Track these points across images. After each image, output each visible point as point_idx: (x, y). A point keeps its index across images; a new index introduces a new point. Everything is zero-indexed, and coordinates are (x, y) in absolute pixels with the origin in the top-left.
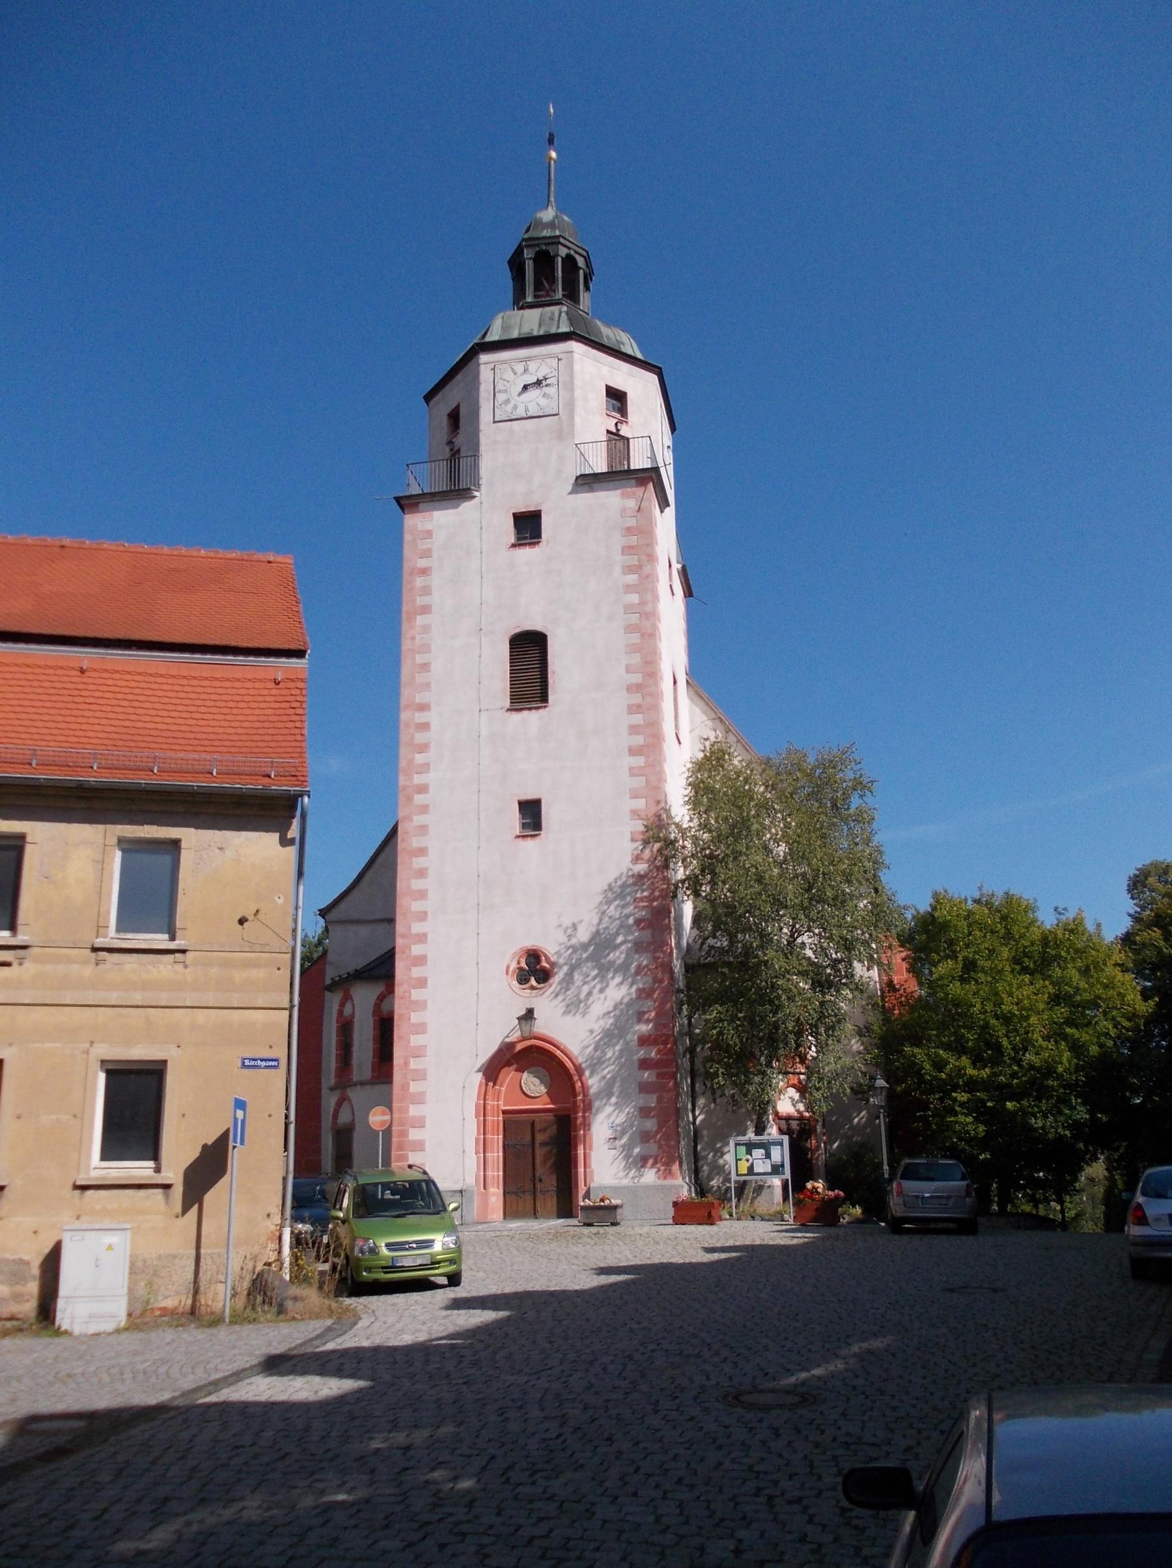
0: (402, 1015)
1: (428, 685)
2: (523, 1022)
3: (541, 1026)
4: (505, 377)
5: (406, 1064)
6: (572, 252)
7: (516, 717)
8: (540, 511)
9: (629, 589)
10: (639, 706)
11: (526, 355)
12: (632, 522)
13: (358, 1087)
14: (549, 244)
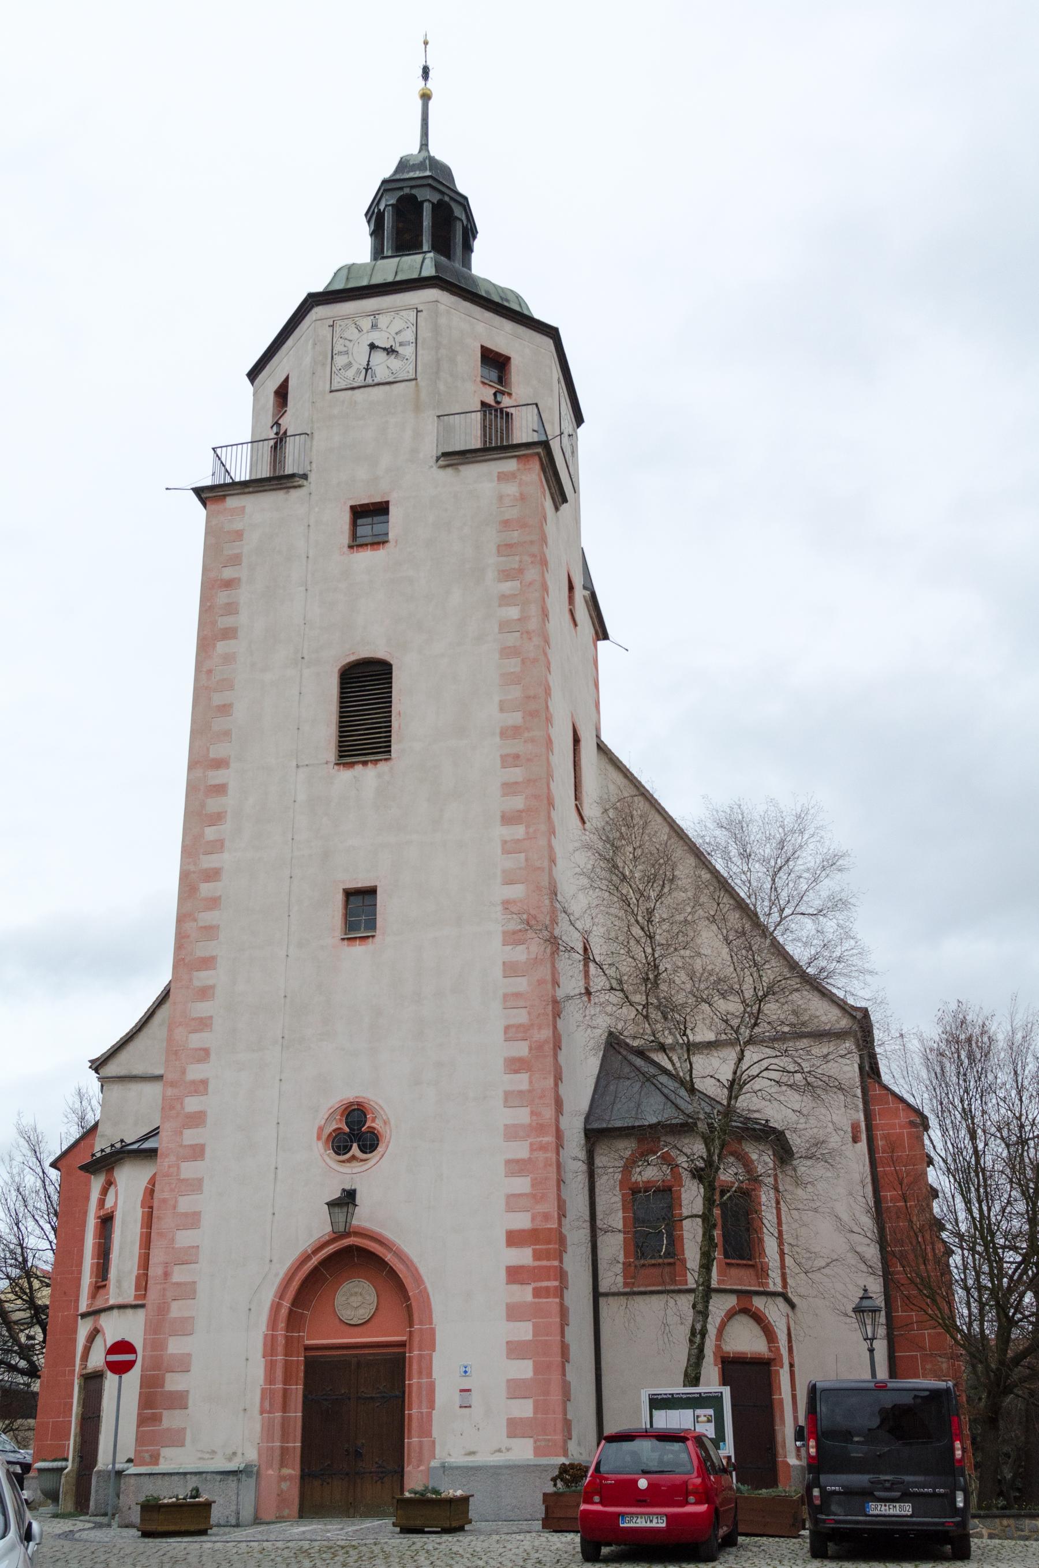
0: (164, 1201)
1: (227, 733)
2: (336, 1210)
3: (364, 1216)
4: (345, 335)
5: (166, 1275)
6: (447, 199)
7: (346, 775)
8: (387, 503)
9: (505, 600)
10: (517, 757)
11: (375, 307)
12: (512, 513)
13: (115, 1312)
14: (412, 187)
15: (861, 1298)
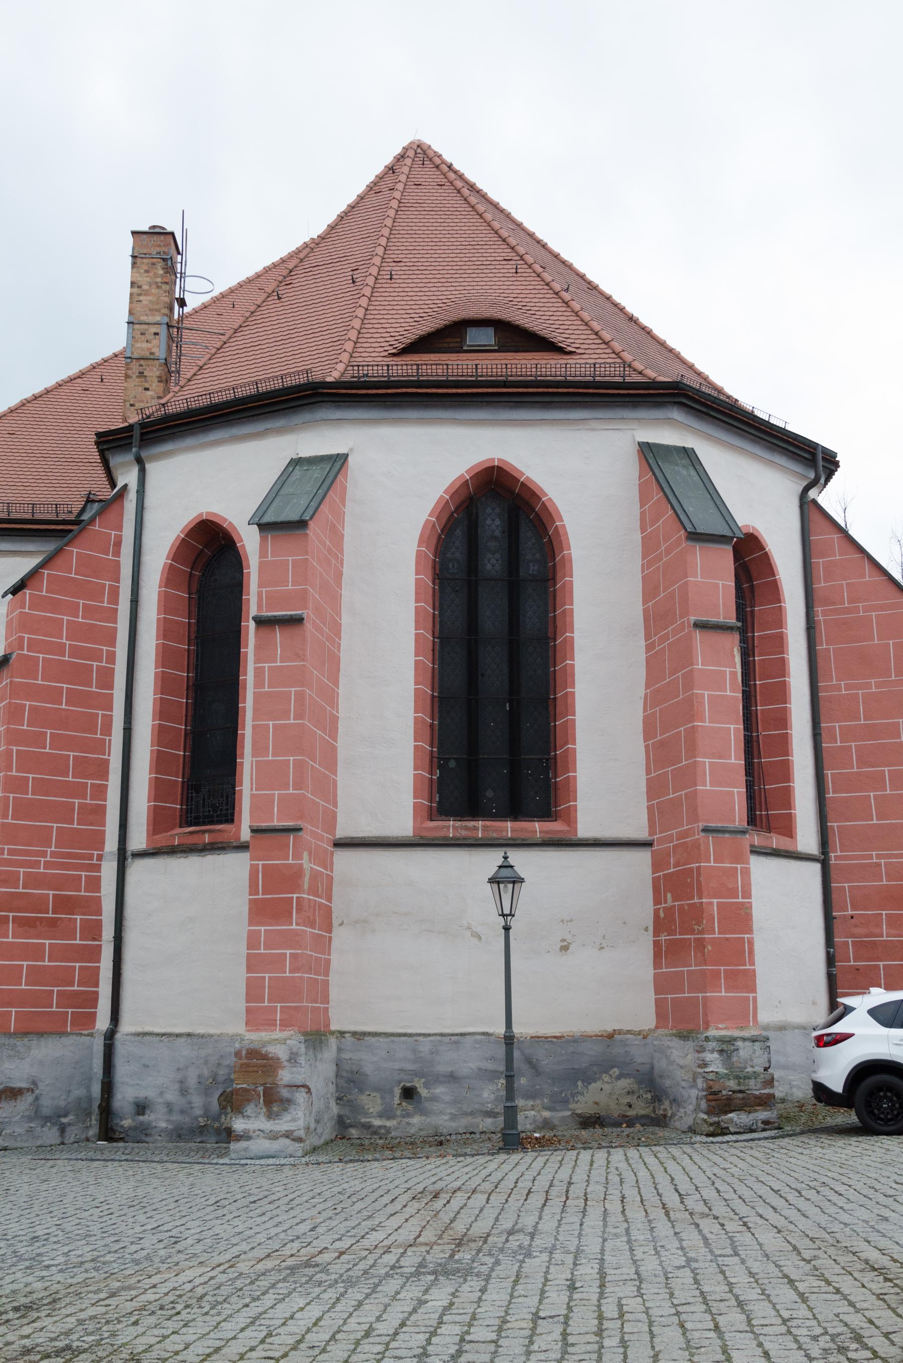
15: (500, 867)
